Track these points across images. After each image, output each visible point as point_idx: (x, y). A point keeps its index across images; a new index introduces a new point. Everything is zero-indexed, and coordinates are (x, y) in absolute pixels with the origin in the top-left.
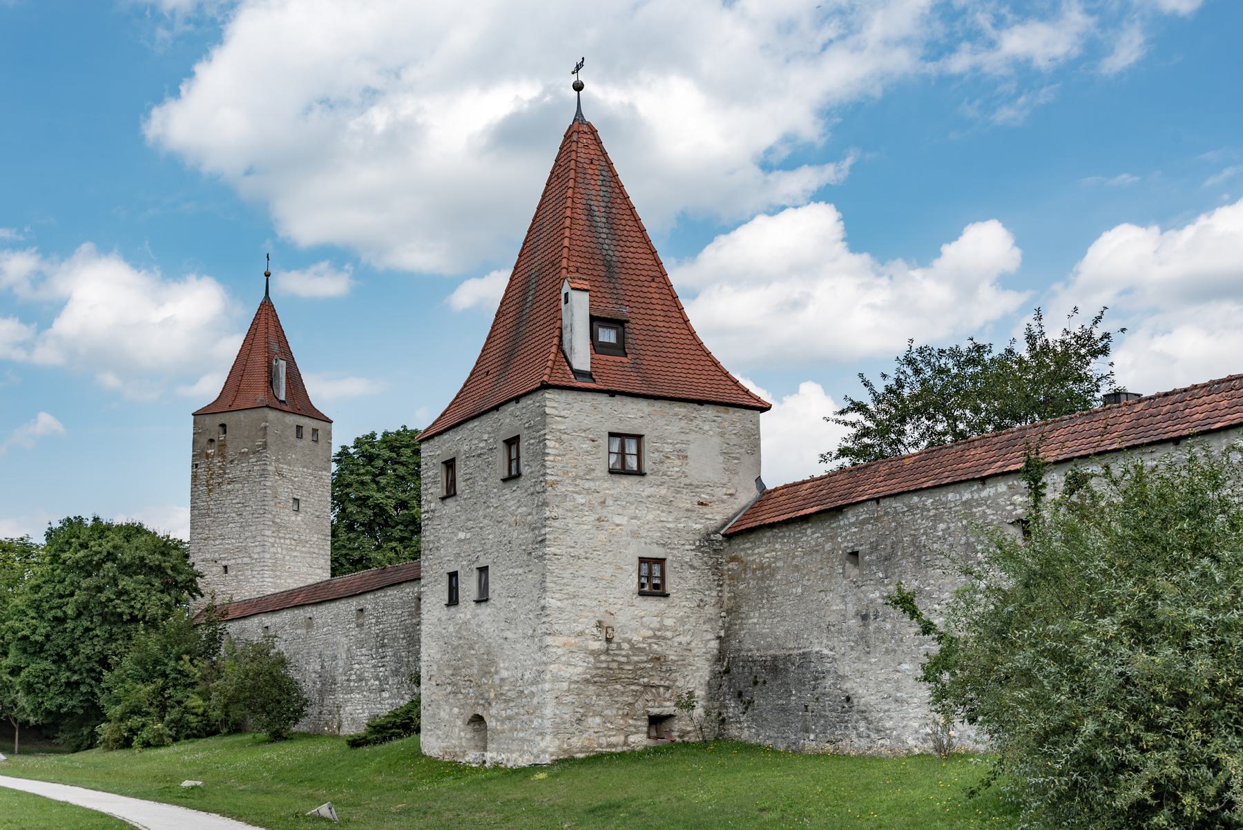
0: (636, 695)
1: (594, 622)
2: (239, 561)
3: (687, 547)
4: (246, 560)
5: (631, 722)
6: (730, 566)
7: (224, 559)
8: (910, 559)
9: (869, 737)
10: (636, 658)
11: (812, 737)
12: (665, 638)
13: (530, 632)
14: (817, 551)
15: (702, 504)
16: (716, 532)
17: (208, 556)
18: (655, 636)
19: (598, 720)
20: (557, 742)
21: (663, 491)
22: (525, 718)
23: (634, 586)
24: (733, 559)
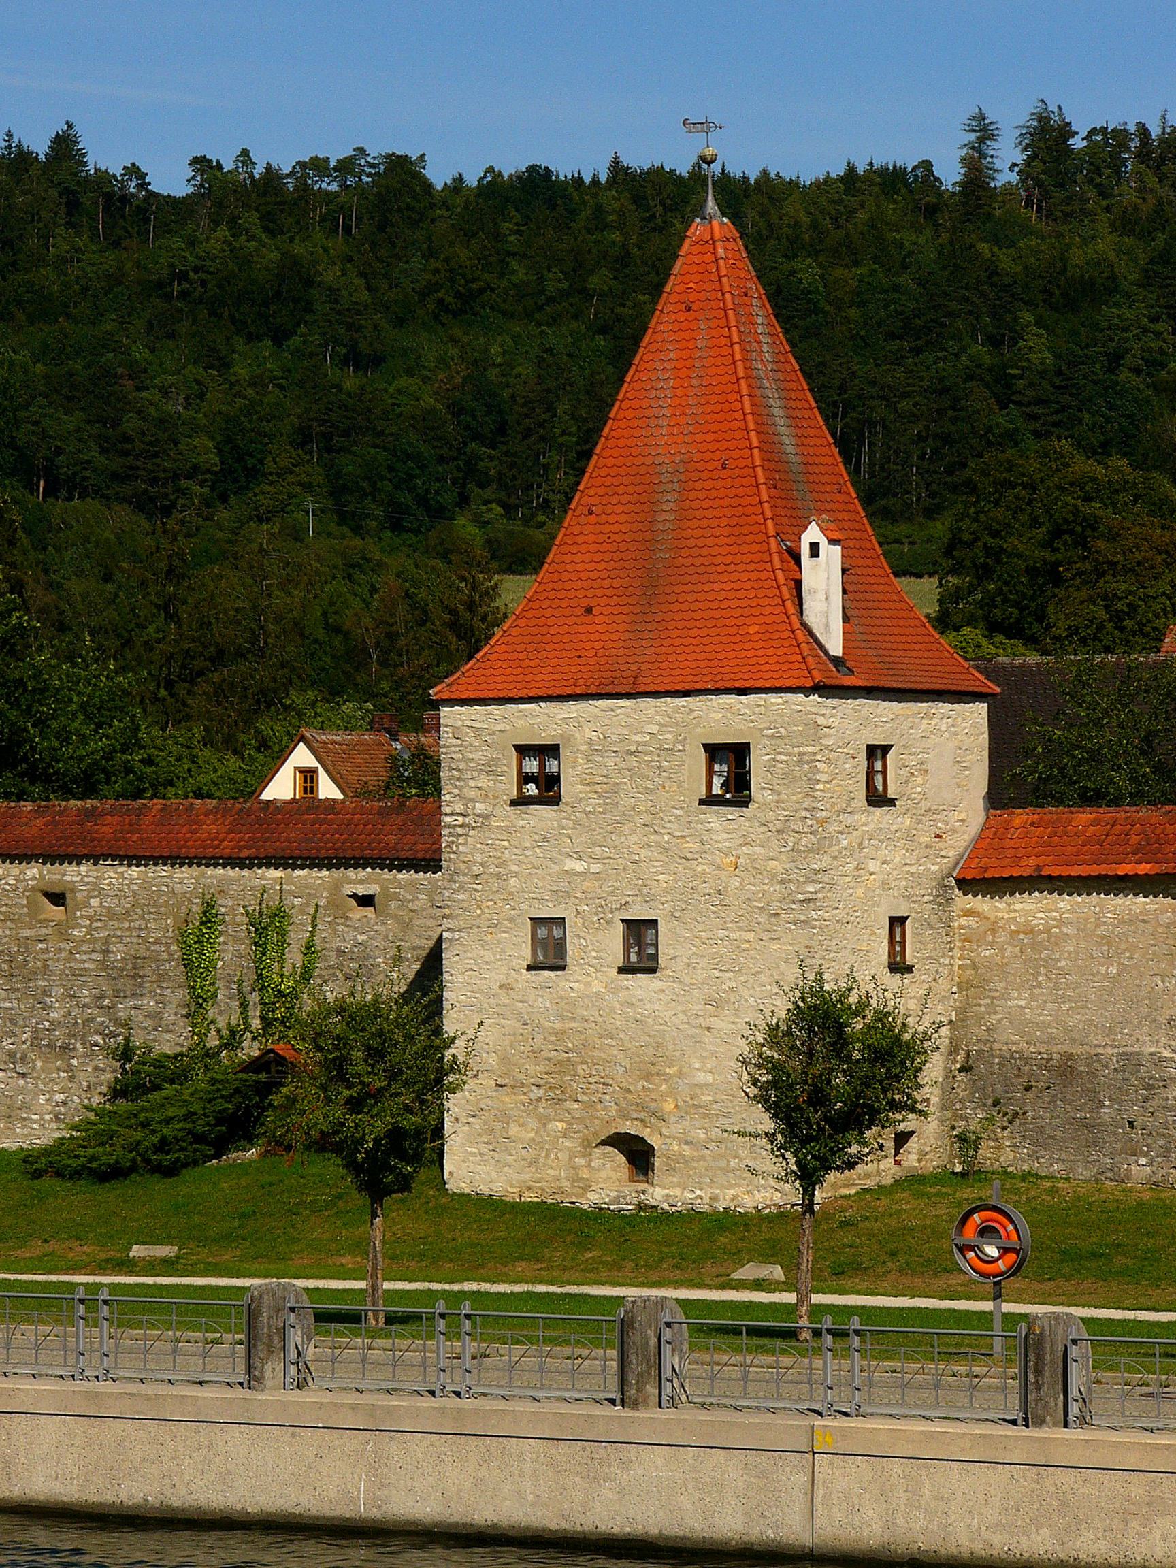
3: (926, 898)
6: (963, 921)
11: (1143, 1161)
14: (1144, 921)
24: (968, 913)
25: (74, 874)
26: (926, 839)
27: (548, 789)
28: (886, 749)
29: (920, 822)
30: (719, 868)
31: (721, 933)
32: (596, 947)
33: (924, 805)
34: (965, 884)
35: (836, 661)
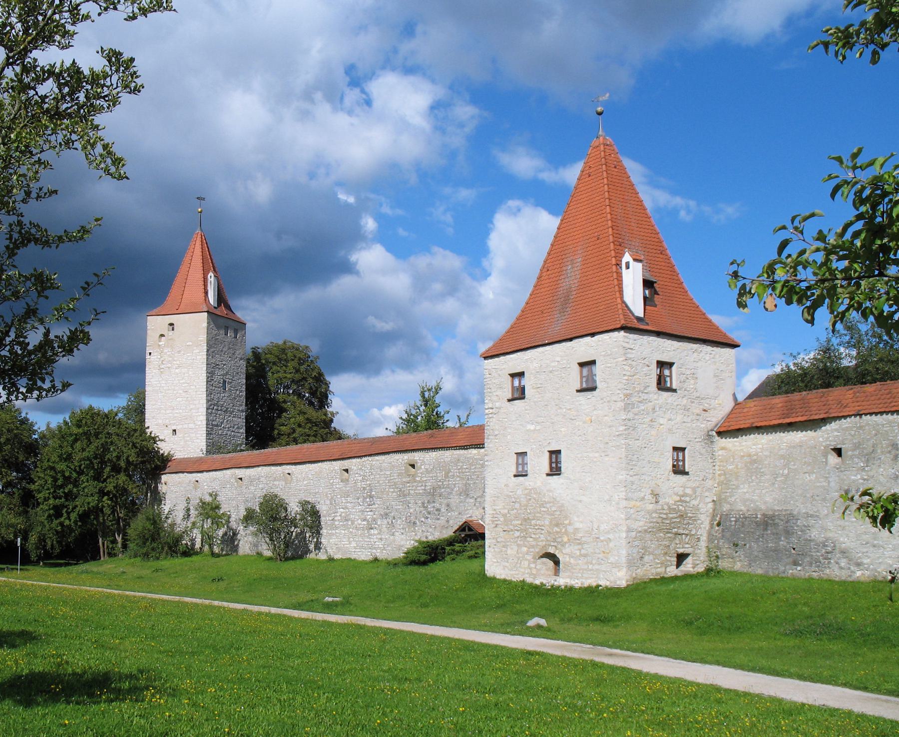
0: (672, 540)
1: (650, 491)
2: (186, 426)
4: (191, 426)
5: (668, 558)
6: (720, 453)
7: (174, 424)
8: (888, 455)
9: (849, 568)
10: (671, 516)
12: (686, 502)
13: (607, 497)
15: (705, 410)
16: (712, 430)
17: (160, 421)
18: (681, 501)
19: (651, 557)
20: (630, 573)
21: (685, 401)
22: (601, 556)
23: (670, 467)
24: (723, 449)
25: (417, 456)
26: (698, 411)
27: (520, 394)
28: (670, 365)
29: (693, 402)
30: (584, 422)
31: (585, 454)
32: (539, 463)
33: (695, 394)
34: (720, 434)
35: (639, 319)
